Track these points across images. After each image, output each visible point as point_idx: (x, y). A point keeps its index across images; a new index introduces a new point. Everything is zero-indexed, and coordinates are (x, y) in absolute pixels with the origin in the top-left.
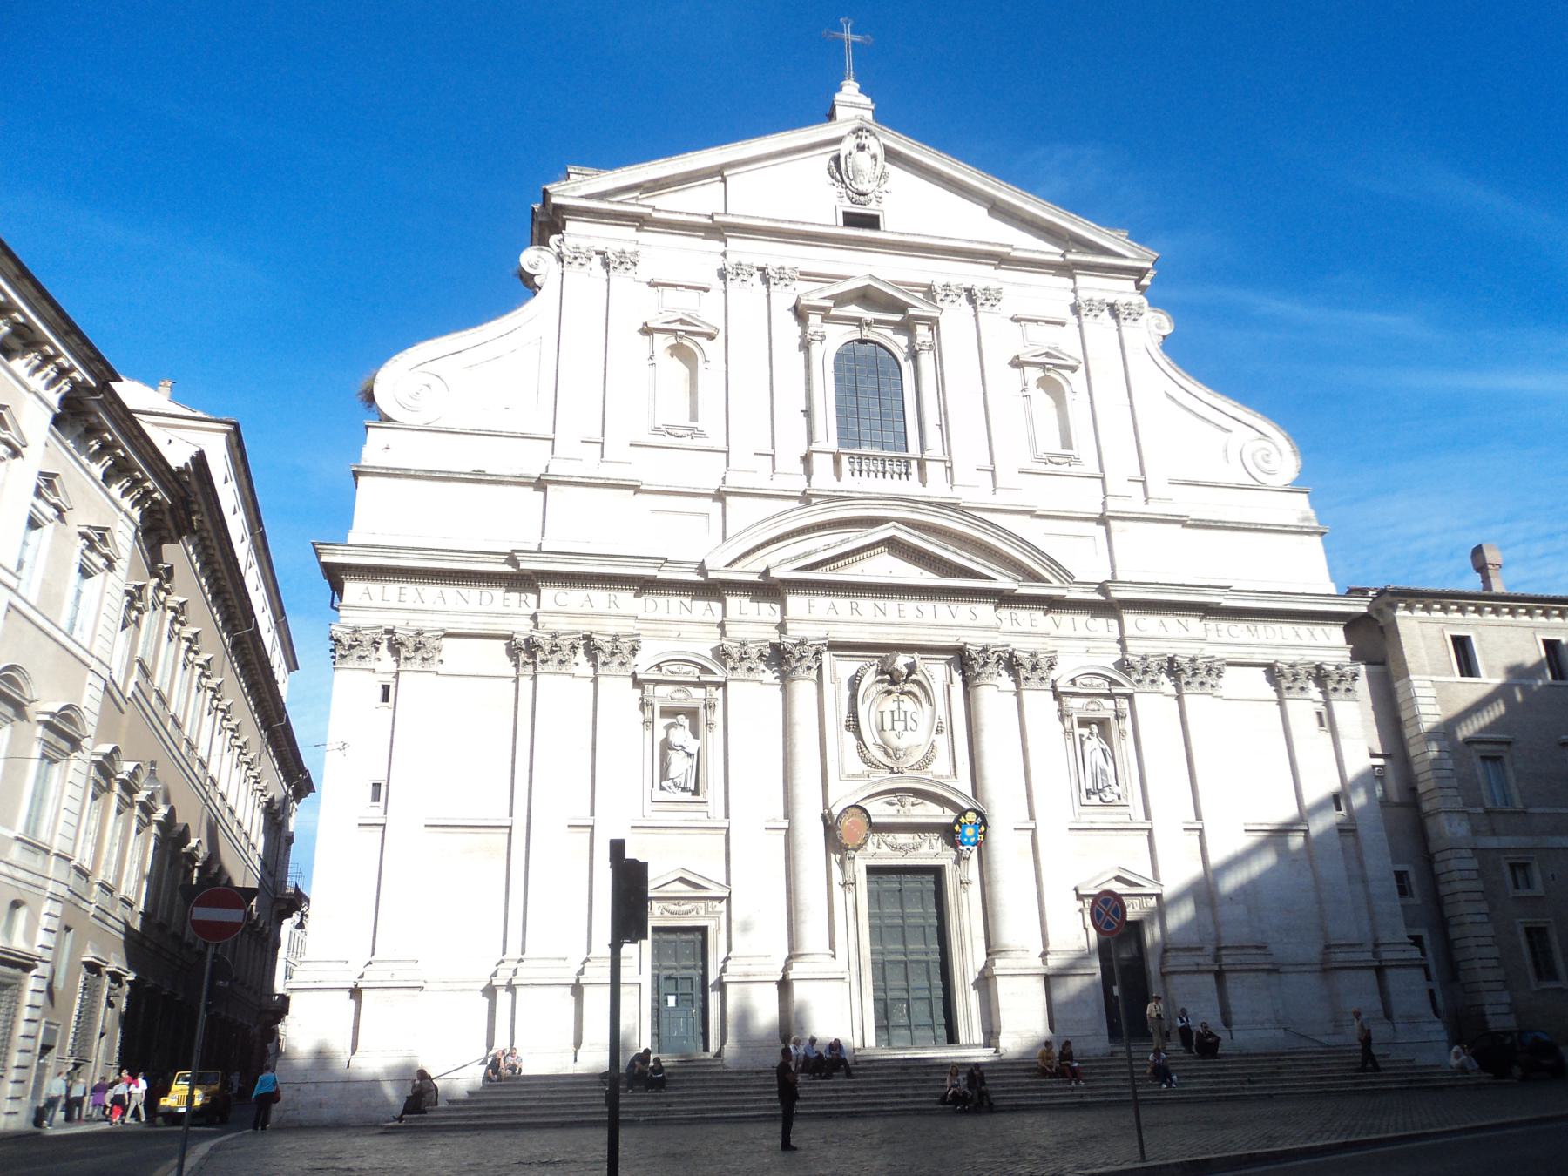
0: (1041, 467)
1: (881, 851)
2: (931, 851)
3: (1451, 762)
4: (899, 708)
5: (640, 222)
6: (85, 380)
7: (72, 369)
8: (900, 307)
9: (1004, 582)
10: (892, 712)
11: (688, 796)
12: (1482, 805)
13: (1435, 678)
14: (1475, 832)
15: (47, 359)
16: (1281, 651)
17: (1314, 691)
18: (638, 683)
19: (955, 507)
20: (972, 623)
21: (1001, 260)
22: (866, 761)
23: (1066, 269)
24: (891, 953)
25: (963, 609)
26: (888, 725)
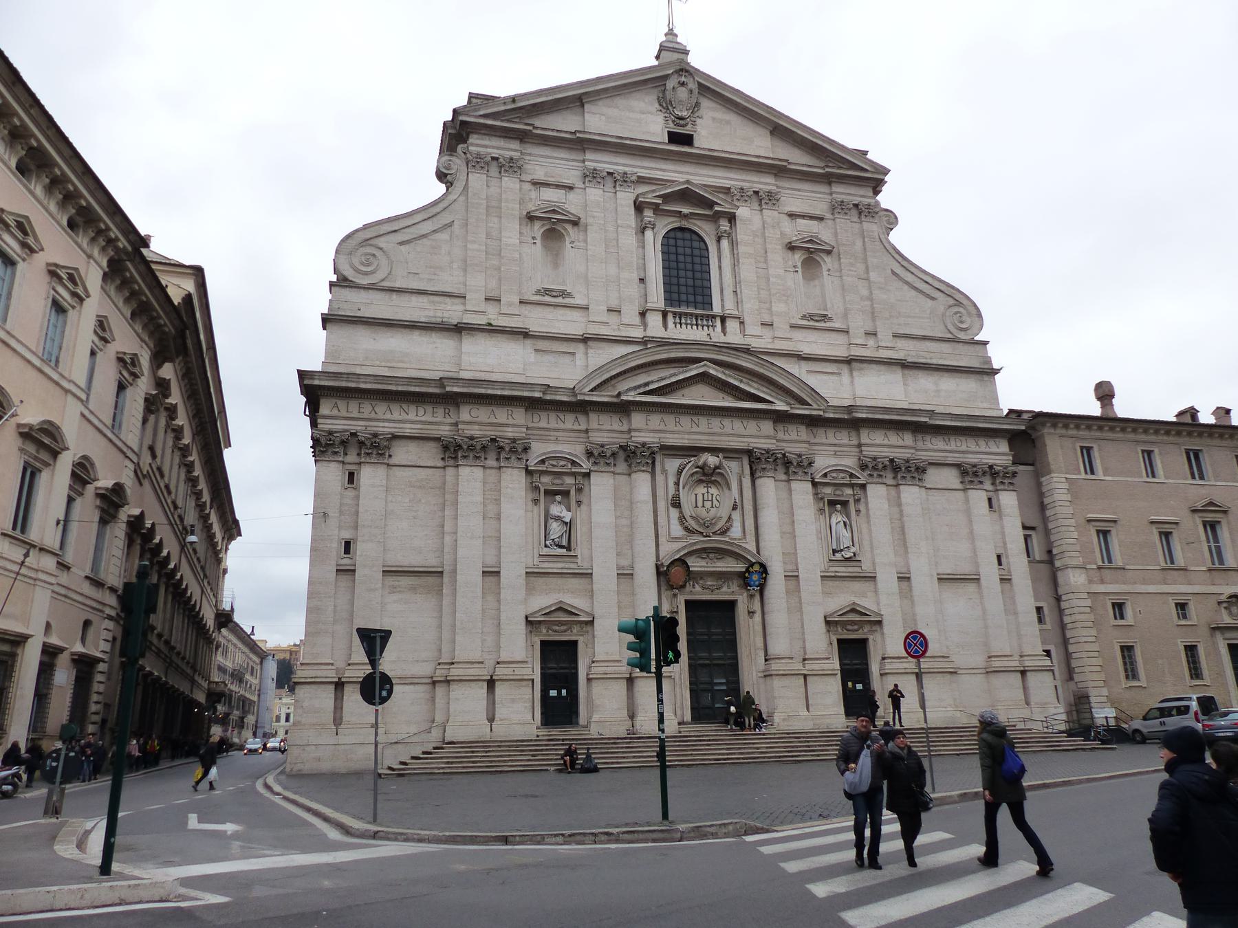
0: (805, 322)
1: (698, 592)
2: (726, 592)
3: (1076, 533)
4: (708, 492)
5: (523, 137)
6: (124, 247)
7: (117, 239)
8: (710, 204)
9: (780, 406)
10: (703, 494)
11: (563, 551)
12: (1096, 563)
13: (1068, 476)
14: (1090, 582)
15: (100, 232)
16: (966, 455)
17: (988, 485)
18: (529, 472)
19: (747, 351)
20: (758, 434)
21: (779, 170)
22: (686, 529)
23: (828, 179)
24: (701, 658)
25: (751, 426)
26: (700, 504)
